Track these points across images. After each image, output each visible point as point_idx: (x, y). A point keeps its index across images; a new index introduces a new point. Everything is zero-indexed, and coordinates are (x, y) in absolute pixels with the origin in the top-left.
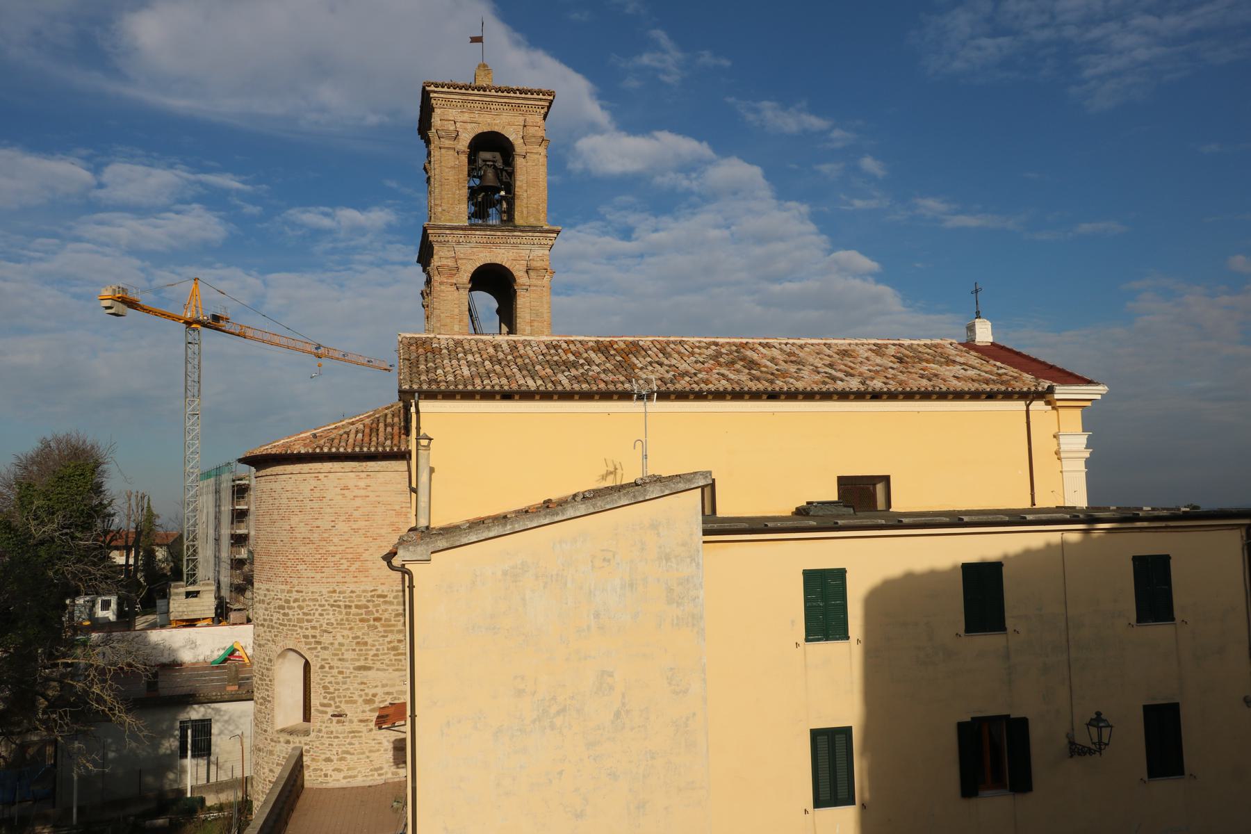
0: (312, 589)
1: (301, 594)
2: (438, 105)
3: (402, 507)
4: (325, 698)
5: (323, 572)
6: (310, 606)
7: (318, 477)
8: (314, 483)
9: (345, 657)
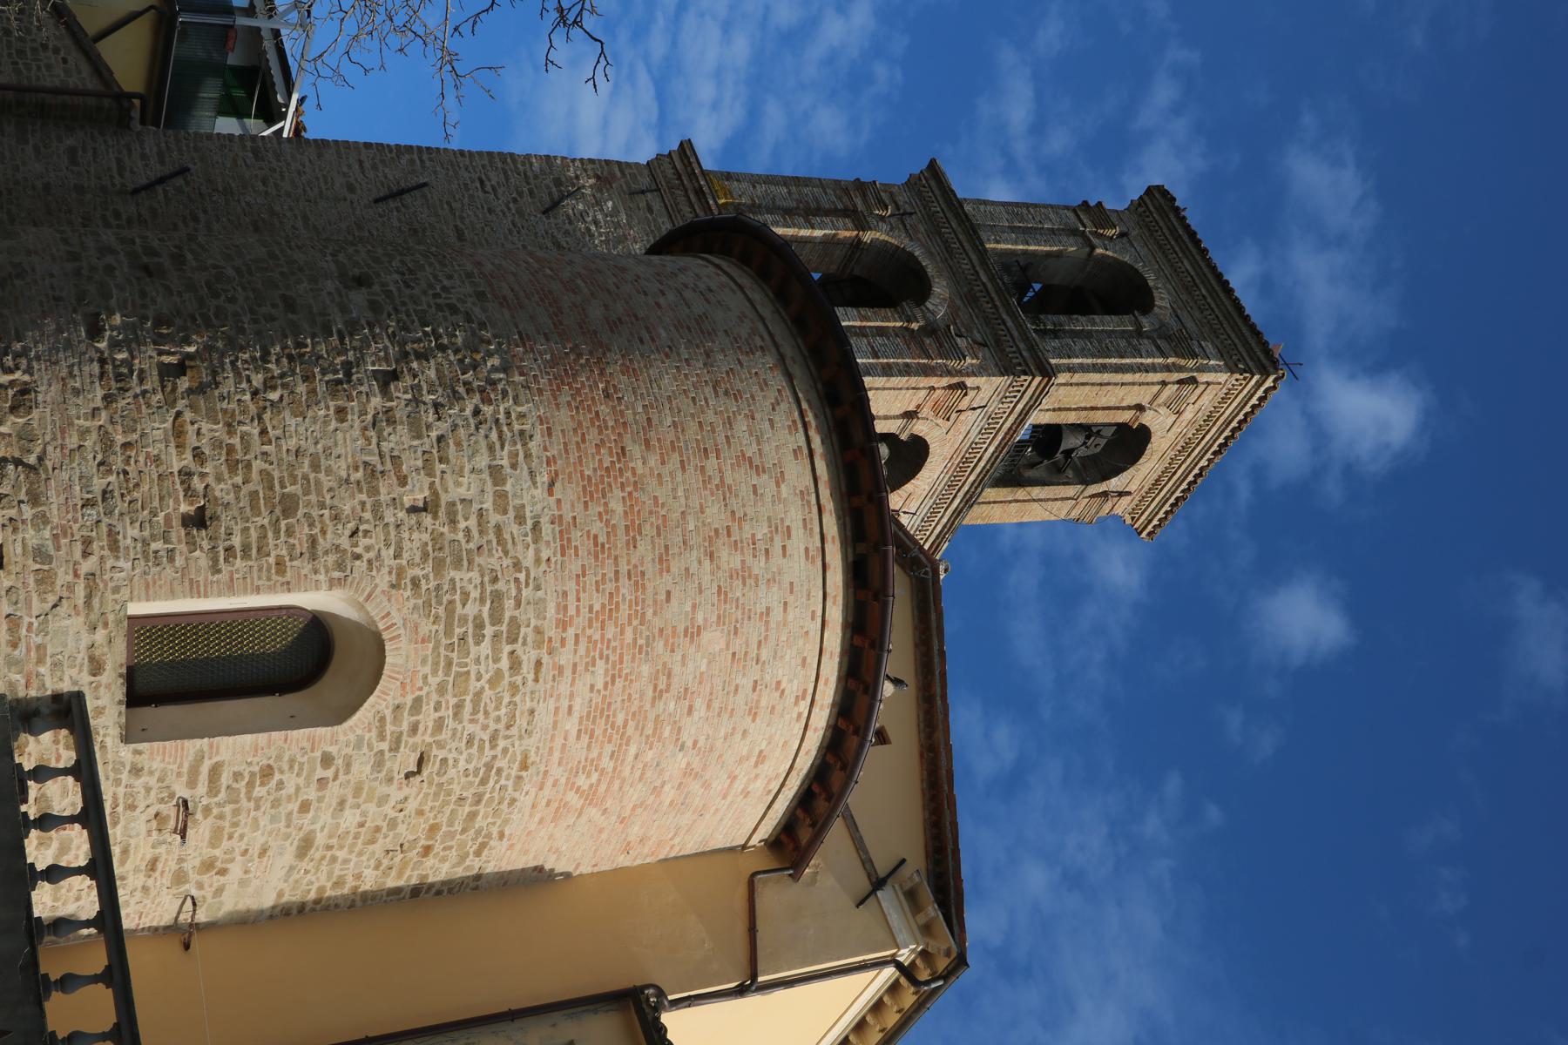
0: (541, 709)
1: (531, 676)
4: (237, 776)
6: (497, 708)
8: (792, 689)
9: (347, 812)
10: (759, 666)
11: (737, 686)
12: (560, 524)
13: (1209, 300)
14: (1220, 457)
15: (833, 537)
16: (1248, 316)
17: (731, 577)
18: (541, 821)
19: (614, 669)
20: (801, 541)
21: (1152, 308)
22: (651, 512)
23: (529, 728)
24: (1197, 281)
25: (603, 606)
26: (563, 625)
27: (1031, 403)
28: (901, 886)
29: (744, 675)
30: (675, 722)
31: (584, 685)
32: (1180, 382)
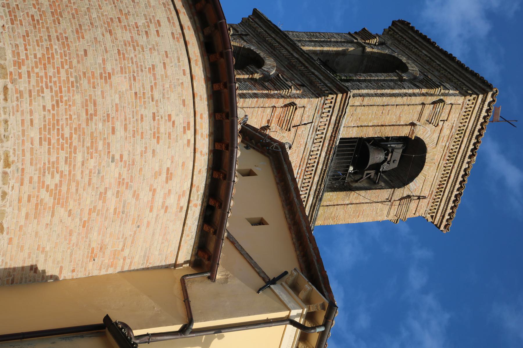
0: (12, 120)
2: (468, 102)
3: (124, 259)
5: (41, 144)
7: (189, 129)
10: (154, 102)
11: (142, 115)
12: (9, 7)
13: (442, 66)
14: (475, 158)
15: (188, 27)
16: (467, 67)
17: (125, 45)
18: (27, 216)
19: (57, 96)
20: (166, 29)
21: (408, 70)
22: (67, 6)
23: (6, 134)
24: (433, 58)
25: (43, 55)
26: (18, 64)
27: (340, 114)
28: (286, 283)
29: (145, 108)
30: (105, 139)
31: (39, 105)
32: (434, 103)
